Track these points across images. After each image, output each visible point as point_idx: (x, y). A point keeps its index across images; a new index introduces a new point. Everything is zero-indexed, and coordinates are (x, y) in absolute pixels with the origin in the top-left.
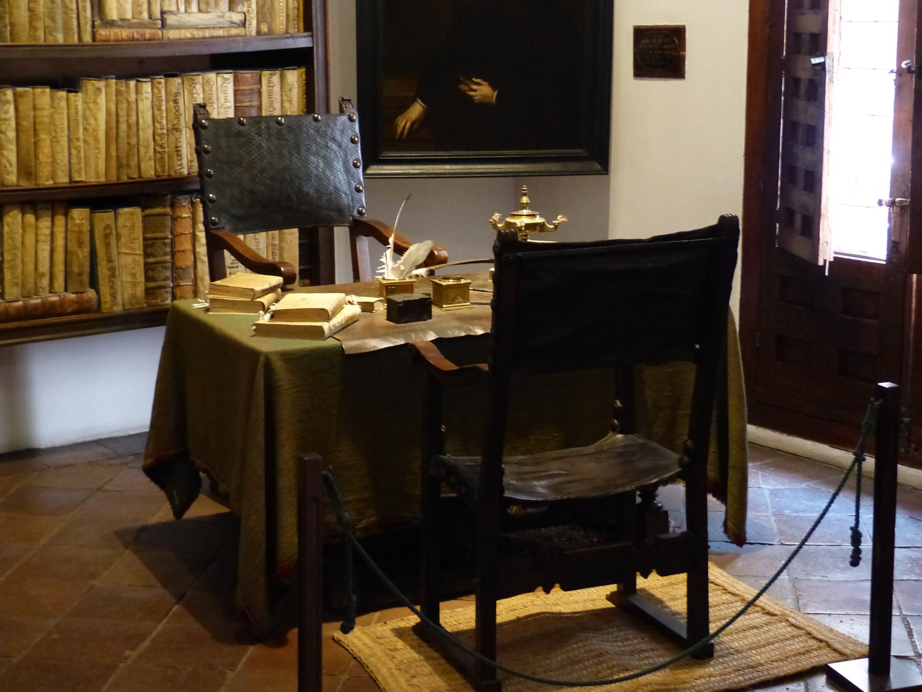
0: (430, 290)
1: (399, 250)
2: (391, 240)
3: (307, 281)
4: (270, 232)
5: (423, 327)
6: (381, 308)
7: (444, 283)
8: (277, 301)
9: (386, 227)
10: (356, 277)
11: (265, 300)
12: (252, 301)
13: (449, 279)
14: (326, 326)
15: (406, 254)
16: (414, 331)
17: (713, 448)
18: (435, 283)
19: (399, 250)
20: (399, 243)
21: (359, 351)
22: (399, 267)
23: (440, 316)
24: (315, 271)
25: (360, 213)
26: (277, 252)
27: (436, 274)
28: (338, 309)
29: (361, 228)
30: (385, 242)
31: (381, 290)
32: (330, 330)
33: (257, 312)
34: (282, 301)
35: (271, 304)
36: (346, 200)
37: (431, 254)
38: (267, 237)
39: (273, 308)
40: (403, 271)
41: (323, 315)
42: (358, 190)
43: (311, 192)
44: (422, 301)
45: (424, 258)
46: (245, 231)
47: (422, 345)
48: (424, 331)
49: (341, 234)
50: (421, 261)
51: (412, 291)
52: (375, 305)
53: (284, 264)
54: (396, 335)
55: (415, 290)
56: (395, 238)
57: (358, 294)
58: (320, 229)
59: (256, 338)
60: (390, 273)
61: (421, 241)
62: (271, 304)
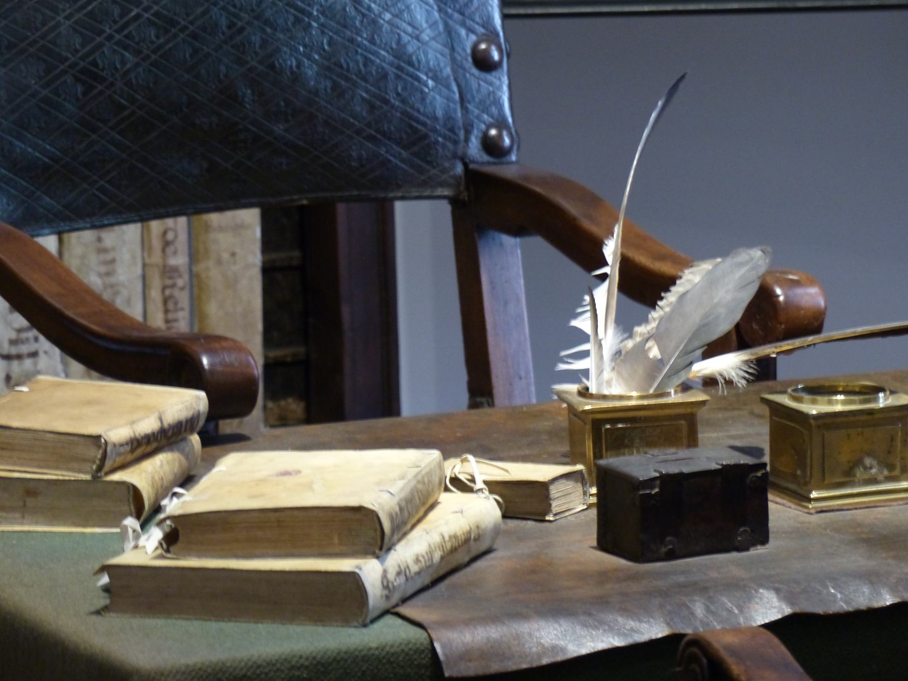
0: (758, 434)
1: (643, 287)
2: (610, 249)
3: (295, 406)
4: (156, 226)
5: (737, 572)
6: (575, 504)
7: (813, 408)
8: (187, 480)
9: (593, 201)
10: (480, 387)
11: (144, 476)
12: (93, 482)
13: (834, 391)
14: (371, 571)
15: (670, 298)
16: (702, 589)
17: (92, 339)
18: (777, 410)
19: (643, 287)
20: (641, 259)
21: (495, 667)
22: (640, 350)
23: (800, 533)
24: (325, 369)
25: (491, 147)
26: (183, 298)
27: (783, 371)
28: (417, 506)
29: (492, 204)
30: (591, 258)
31: (574, 437)
32: (386, 585)
33: (117, 522)
34: (205, 482)
35: (166, 491)
36: (438, 101)
37: (763, 300)
38: (145, 243)
39: (172, 507)
40: (659, 364)
41: (361, 528)
42: (484, 63)
43: (310, 71)
44: (730, 473)
45: (738, 316)
46: (65, 220)
47: (730, 639)
48: (741, 589)
49: (420, 229)
50: (724, 326)
51: (692, 441)
52: (554, 491)
53: (212, 342)
54: (632, 605)
55: (705, 435)
56: (626, 241)
57: (487, 452)
58: (341, 208)
59: (113, 620)
60: (607, 374)
61: (722, 250)
62: (166, 491)
